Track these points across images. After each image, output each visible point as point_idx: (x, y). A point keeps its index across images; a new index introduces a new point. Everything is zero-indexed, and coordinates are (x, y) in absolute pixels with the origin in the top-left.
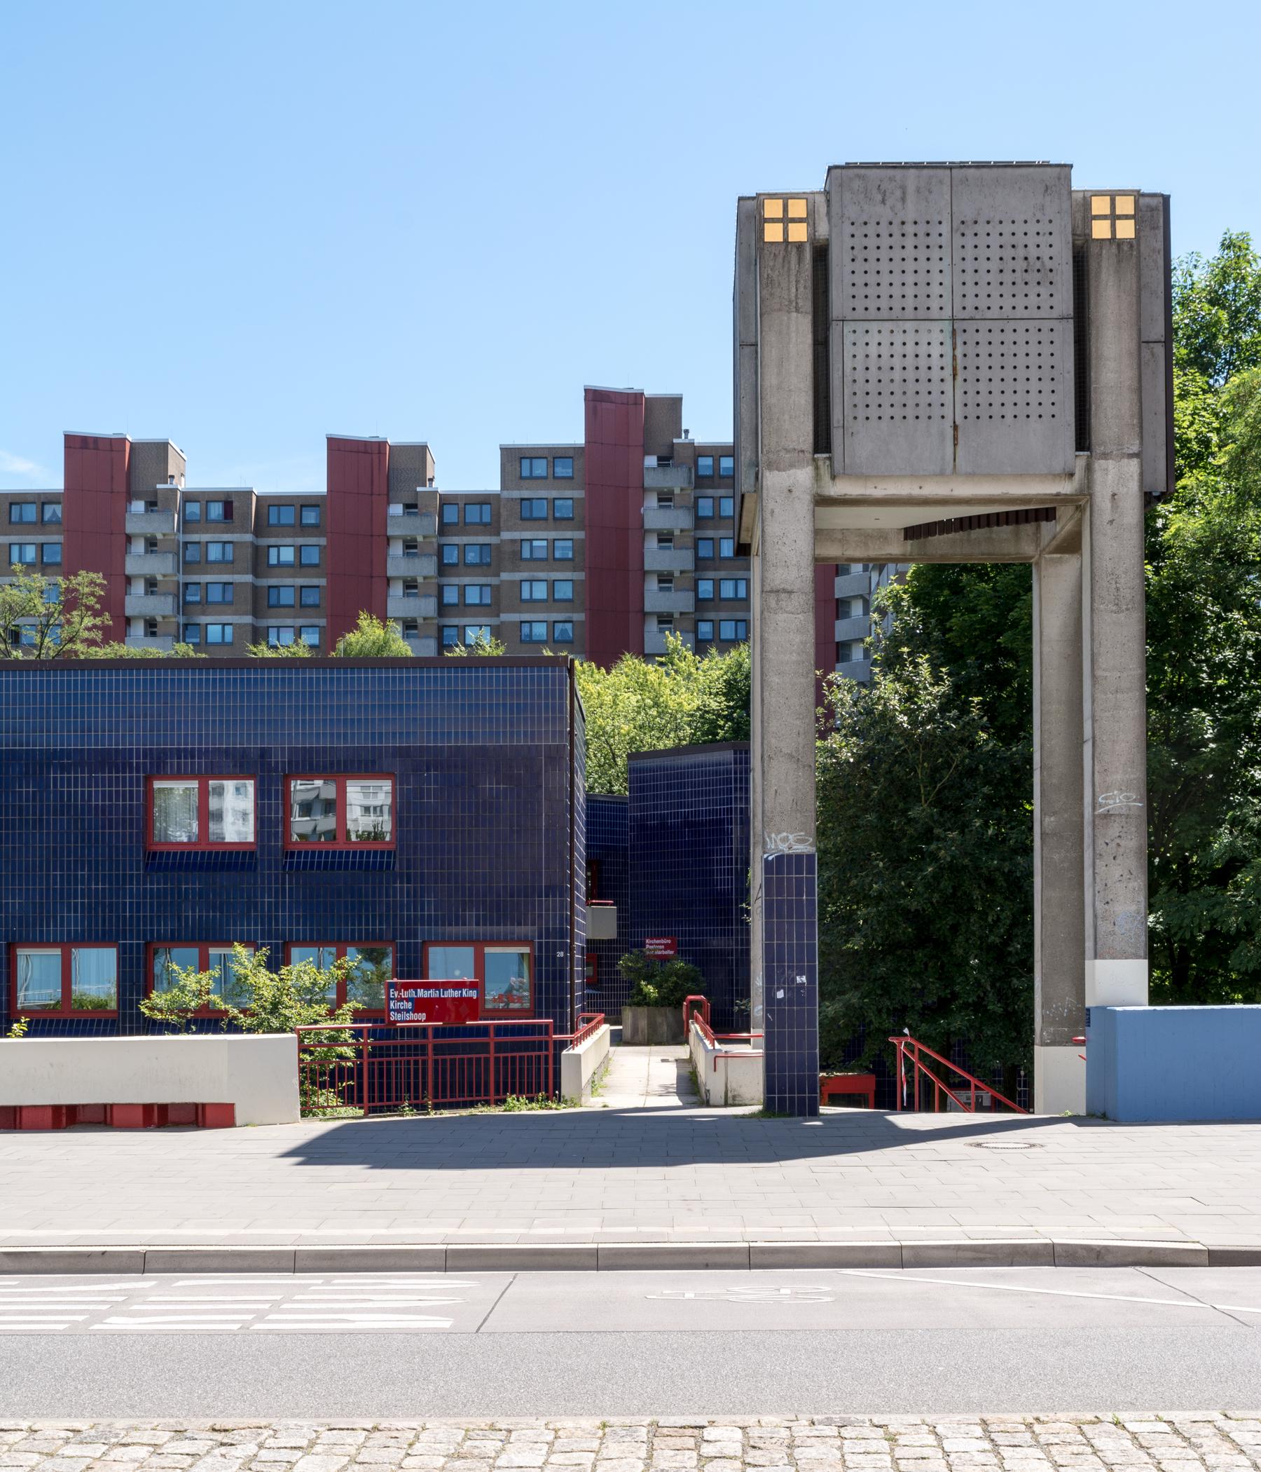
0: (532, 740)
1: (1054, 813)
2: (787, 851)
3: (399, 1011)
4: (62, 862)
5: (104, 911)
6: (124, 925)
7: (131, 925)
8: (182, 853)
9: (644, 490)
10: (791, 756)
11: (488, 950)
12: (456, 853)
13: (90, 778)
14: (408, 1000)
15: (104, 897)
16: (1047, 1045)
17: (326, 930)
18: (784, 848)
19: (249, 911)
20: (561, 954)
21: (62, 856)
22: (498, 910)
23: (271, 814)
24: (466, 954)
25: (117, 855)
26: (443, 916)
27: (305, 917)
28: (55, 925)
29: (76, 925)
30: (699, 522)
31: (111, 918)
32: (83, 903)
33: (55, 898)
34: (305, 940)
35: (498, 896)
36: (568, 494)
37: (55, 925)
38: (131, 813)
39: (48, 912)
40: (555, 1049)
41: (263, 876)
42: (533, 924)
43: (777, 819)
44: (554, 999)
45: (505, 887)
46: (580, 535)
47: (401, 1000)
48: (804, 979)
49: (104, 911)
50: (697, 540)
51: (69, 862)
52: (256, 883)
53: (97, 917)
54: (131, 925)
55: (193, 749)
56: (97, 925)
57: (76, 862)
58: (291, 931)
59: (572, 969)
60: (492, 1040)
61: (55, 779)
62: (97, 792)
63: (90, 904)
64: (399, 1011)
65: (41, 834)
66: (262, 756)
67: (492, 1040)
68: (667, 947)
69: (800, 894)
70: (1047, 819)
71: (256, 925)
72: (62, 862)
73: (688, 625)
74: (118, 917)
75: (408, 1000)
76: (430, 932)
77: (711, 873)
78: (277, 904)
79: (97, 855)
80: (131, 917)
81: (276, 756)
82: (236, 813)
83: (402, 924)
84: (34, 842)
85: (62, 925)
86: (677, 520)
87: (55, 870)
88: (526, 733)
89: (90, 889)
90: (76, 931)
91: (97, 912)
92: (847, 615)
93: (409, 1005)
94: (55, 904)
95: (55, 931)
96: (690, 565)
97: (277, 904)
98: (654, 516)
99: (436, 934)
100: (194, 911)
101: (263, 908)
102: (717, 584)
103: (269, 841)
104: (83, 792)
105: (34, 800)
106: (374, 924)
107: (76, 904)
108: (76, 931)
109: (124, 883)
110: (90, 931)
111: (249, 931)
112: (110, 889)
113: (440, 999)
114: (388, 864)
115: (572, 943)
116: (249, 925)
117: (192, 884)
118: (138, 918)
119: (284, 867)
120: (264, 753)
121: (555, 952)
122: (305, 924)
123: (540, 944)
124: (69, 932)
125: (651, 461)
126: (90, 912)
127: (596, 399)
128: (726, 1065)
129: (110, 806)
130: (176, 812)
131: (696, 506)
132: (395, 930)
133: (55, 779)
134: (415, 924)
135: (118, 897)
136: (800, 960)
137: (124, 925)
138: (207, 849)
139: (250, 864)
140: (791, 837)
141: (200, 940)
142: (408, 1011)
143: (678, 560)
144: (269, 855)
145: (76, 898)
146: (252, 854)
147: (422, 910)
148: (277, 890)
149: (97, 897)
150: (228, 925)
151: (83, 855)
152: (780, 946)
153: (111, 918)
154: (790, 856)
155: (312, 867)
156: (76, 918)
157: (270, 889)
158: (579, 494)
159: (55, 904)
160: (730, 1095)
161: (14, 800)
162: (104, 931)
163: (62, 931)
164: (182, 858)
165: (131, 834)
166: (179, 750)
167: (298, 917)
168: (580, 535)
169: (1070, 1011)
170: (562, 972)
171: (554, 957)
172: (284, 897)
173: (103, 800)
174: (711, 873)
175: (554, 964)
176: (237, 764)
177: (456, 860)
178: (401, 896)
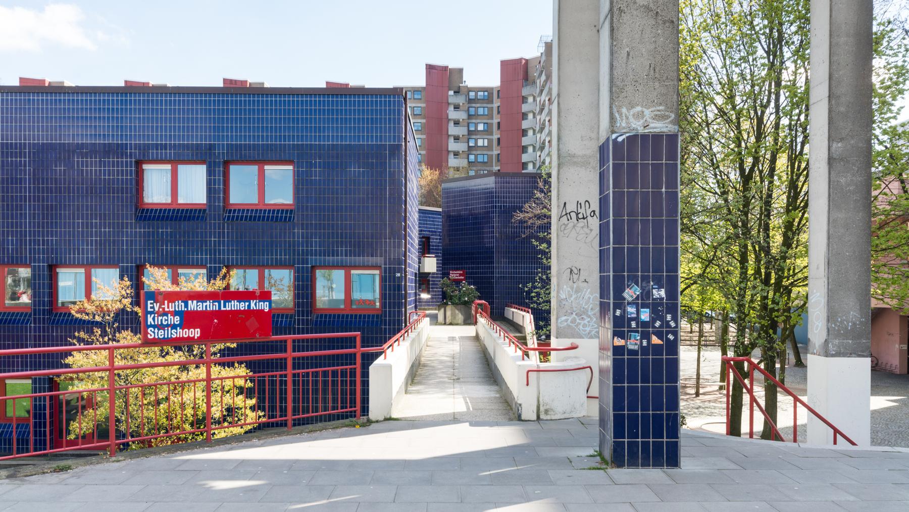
0: (381, 141)
1: (842, 140)
2: (641, 130)
3: (161, 327)
4: (83, 214)
5: (109, 245)
6: (122, 254)
7: (127, 254)
8: (161, 210)
9: (449, 104)
10: (647, 8)
11: (353, 272)
12: (333, 211)
13: (100, 161)
14: (175, 313)
15: (109, 236)
16: (833, 356)
17: (250, 259)
18: (638, 126)
19: (202, 246)
20: (398, 275)
21: (83, 210)
22: (359, 247)
23: (218, 186)
24: (339, 275)
25: (118, 210)
26: (324, 251)
27: (237, 250)
28: (79, 254)
29: (92, 254)
30: (470, 116)
31: (114, 249)
32: (96, 241)
33: (78, 237)
34: (237, 264)
35: (359, 238)
36: (419, 105)
37: (79, 254)
38: (127, 184)
39: (74, 245)
40: (363, 359)
41: (210, 224)
42: (381, 256)
43: (630, 89)
44: (394, 303)
45: (363, 233)
46: (424, 121)
47: (165, 314)
48: (663, 293)
49: (109, 245)
50: (468, 124)
51: (87, 214)
52: (206, 228)
53: (105, 249)
54: (127, 254)
55: (166, 144)
56: (105, 254)
57: (91, 214)
58: (228, 259)
59: (405, 285)
60: (290, 355)
61: (78, 162)
62: (105, 170)
63: (101, 240)
64: (161, 327)
65: (69, 197)
66: (210, 149)
67: (290, 355)
68: (461, 275)
69: (657, 184)
70: (834, 145)
71: (206, 254)
72: (83, 214)
73: (465, 156)
74: (118, 249)
75: (175, 313)
76: (316, 260)
77: (483, 238)
78: (219, 241)
79: (105, 210)
80: (127, 249)
81: (219, 149)
82: (193, 186)
83: (298, 255)
84: (65, 201)
85: (83, 254)
86: (461, 115)
87: (78, 219)
88: (376, 136)
89: (100, 232)
90: (92, 258)
91: (105, 246)
92: (526, 152)
93: (177, 320)
94: (78, 240)
95: (78, 258)
96: (466, 133)
97: (219, 241)
98: (453, 114)
99: (320, 261)
100: (167, 246)
101: (210, 245)
102: (476, 140)
103: (215, 202)
104: (96, 170)
105: (65, 175)
106: (281, 255)
107: (92, 241)
108: (92, 258)
109: (123, 228)
110: (101, 258)
111: (202, 259)
112: (114, 232)
113: (220, 311)
114: (290, 217)
115: (405, 268)
116: (202, 254)
117: (166, 229)
118: (131, 249)
119: (224, 219)
120: (211, 147)
121: (394, 273)
122: (237, 255)
123: (385, 268)
124: (87, 258)
125: (451, 93)
126: (101, 245)
127: (430, 69)
128: (538, 379)
129: (113, 179)
130: (157, 187)
131: (468, 110)
132: (294, 259)
133: (78, 162)
134: (307, 255)
135: (118, 236)
136: (657, 269)
137: (122, 254)
138: (177, 207)
139: (203, 217)
140: (647, 112)
141: (171, 264)
142: (174, 327)
143: (461, 131)
144: (215, 211)
145: (92, 237)
146: (205, 210)
147: (312, 246)
148: (219, 233)
149: (105, 236)
150: (189, 254)
151: (96, 210)
152: (632, 252)
153: (114, 249)
154: (645, 137)
155: (241, 219)
156: (92, 249)
157: (215, 232)
158: (424, 105)
159: (78, 240)
160: (542, 409)
161: (52, 175)
162: (109, 258)
163: (83, 258)
164: (160, 212)
165: (127, 197)
166: (157, 144)
167: (233, 250)
168: (424, 105)
169: (854, 324)
170: (399, 286)
171: (394, 276)
172: (224, 237)
173: (109, 175)
174: (483, 238)
175: (394, 281)
176: (195, 155)
177: (333, 215)
178: (298, 238)
